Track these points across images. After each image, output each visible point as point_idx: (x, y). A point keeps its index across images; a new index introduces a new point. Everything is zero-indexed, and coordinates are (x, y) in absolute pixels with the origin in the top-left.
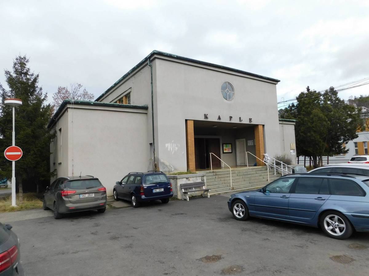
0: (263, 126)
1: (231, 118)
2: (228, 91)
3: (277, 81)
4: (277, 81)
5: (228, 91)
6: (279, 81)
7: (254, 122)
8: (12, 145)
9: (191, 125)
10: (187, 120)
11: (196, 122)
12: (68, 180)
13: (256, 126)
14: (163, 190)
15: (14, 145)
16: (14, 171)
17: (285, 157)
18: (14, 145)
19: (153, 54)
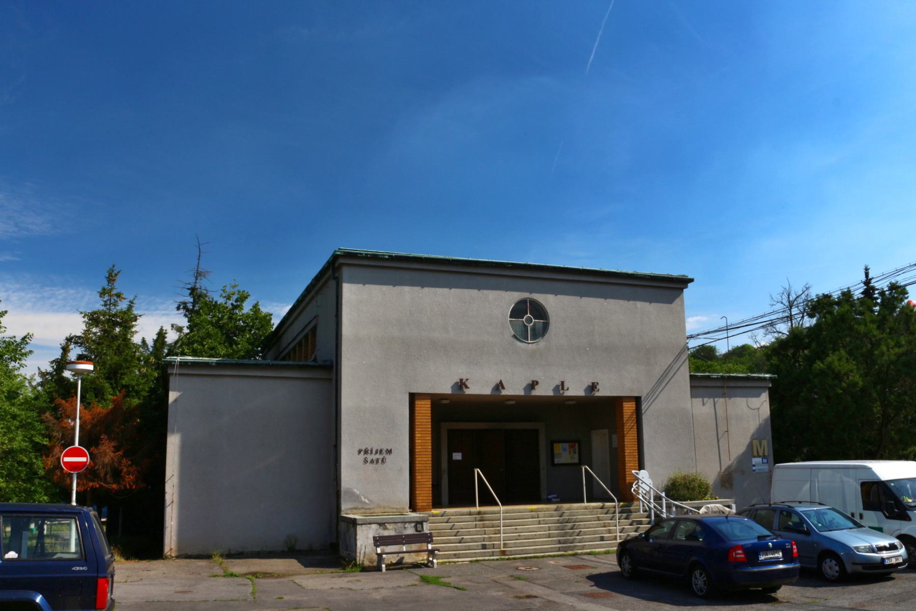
0: (638, 400)
1: (533, 385)
2: (531, 320)
3: (684, 282)
4: (684, 282)
5: (531, 320)
6: (692, 280)
7: (603, 391)
8: (73, 444)
9: (424, 408)
10: (329, 371)
11: (436, 400)
12: (747, 516)
13: (615, 402)
14: (679, 537)
15: (77, 445)
16: (168, 498)
17: (109, 566)
18: (77, 445)
19: (335, 257)
